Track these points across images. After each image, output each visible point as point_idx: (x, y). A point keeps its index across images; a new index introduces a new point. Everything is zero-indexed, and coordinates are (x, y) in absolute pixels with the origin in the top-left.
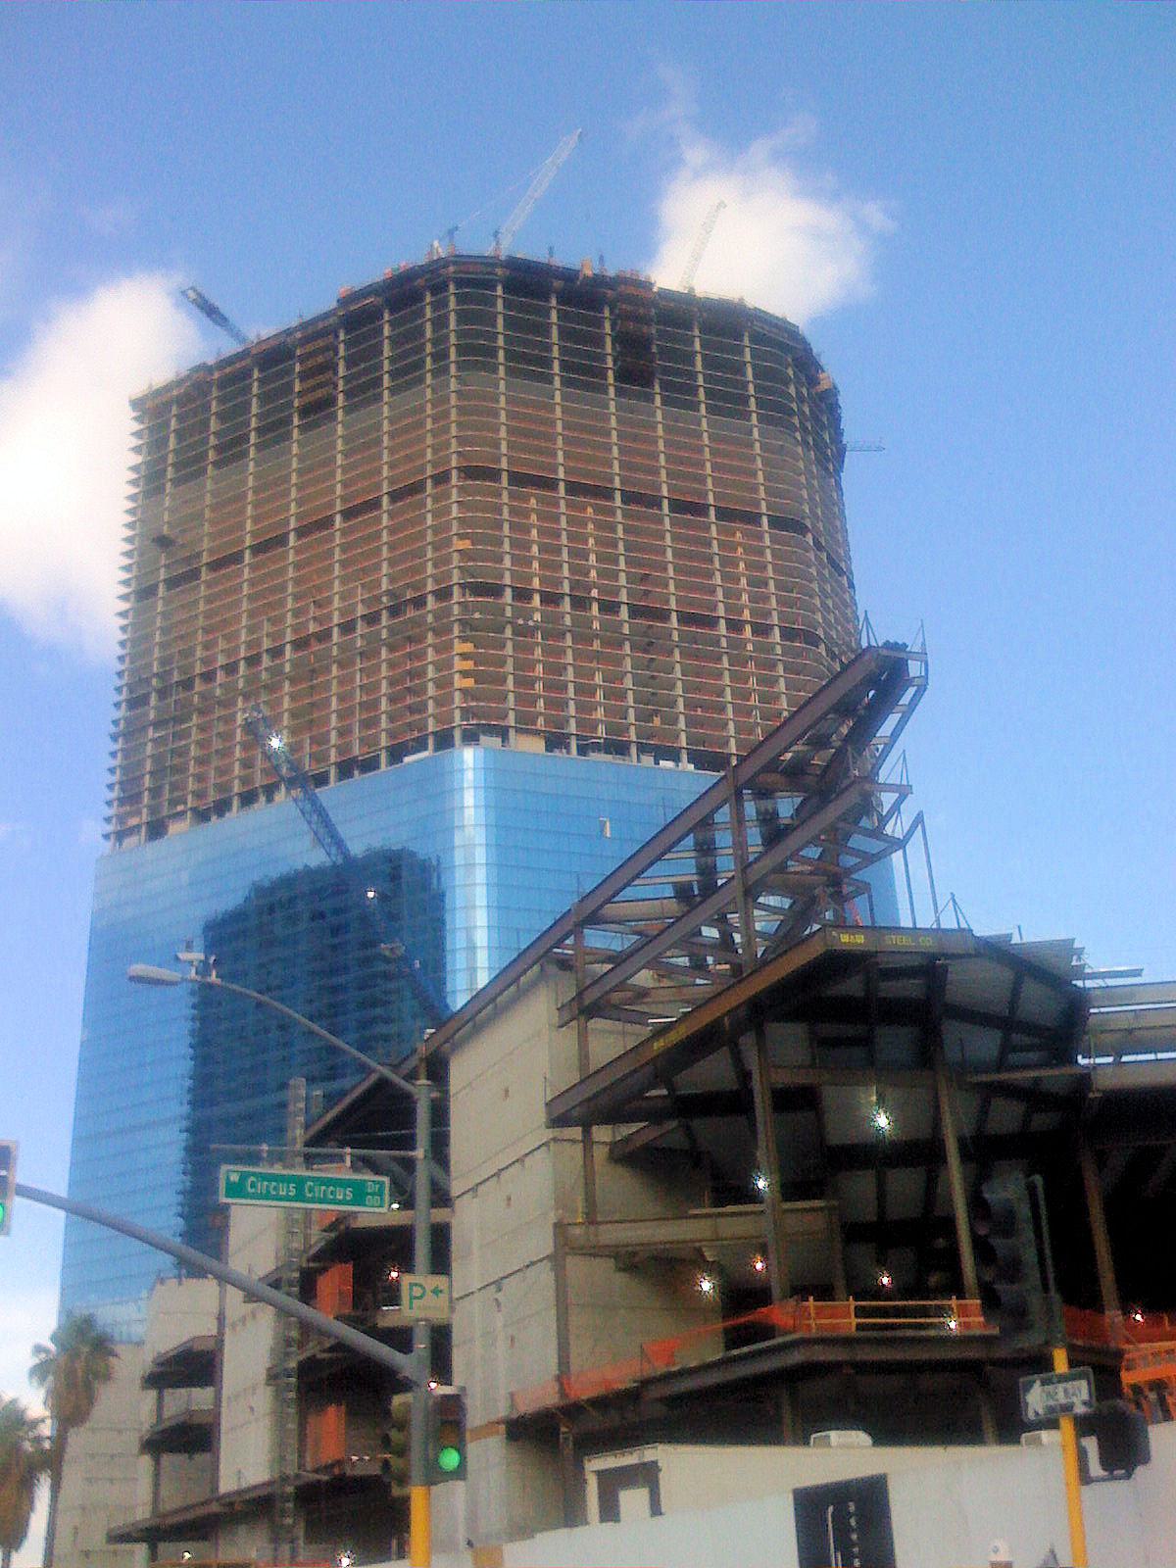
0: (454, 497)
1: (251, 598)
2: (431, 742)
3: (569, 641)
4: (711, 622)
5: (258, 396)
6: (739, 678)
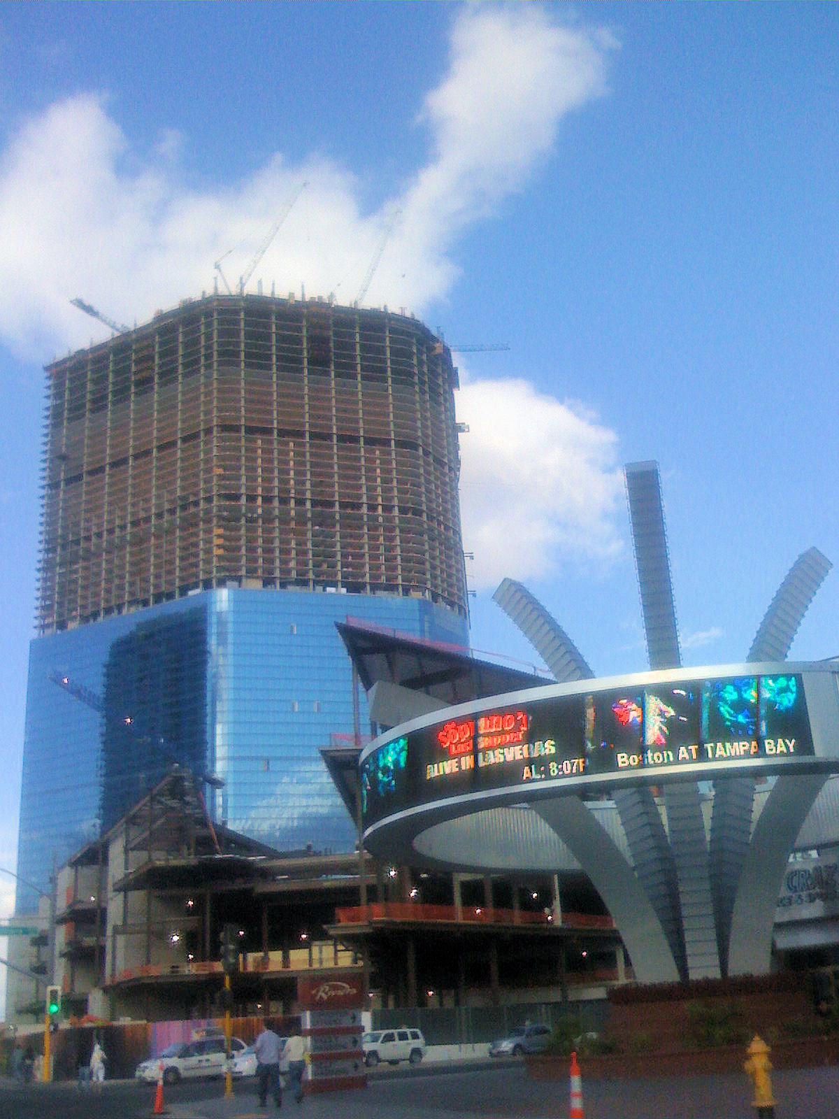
0: (215, 443)
1: (110, 494)
2: (201, 585)
3: (277, 523)
4: (357, 506)
5: (113, 371)
6: (373, 538)
